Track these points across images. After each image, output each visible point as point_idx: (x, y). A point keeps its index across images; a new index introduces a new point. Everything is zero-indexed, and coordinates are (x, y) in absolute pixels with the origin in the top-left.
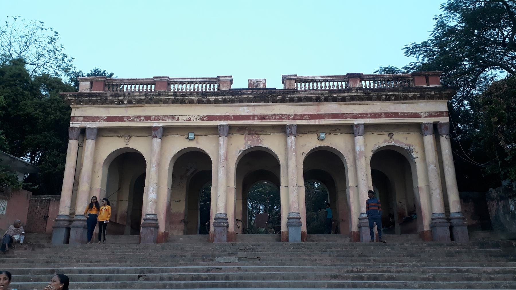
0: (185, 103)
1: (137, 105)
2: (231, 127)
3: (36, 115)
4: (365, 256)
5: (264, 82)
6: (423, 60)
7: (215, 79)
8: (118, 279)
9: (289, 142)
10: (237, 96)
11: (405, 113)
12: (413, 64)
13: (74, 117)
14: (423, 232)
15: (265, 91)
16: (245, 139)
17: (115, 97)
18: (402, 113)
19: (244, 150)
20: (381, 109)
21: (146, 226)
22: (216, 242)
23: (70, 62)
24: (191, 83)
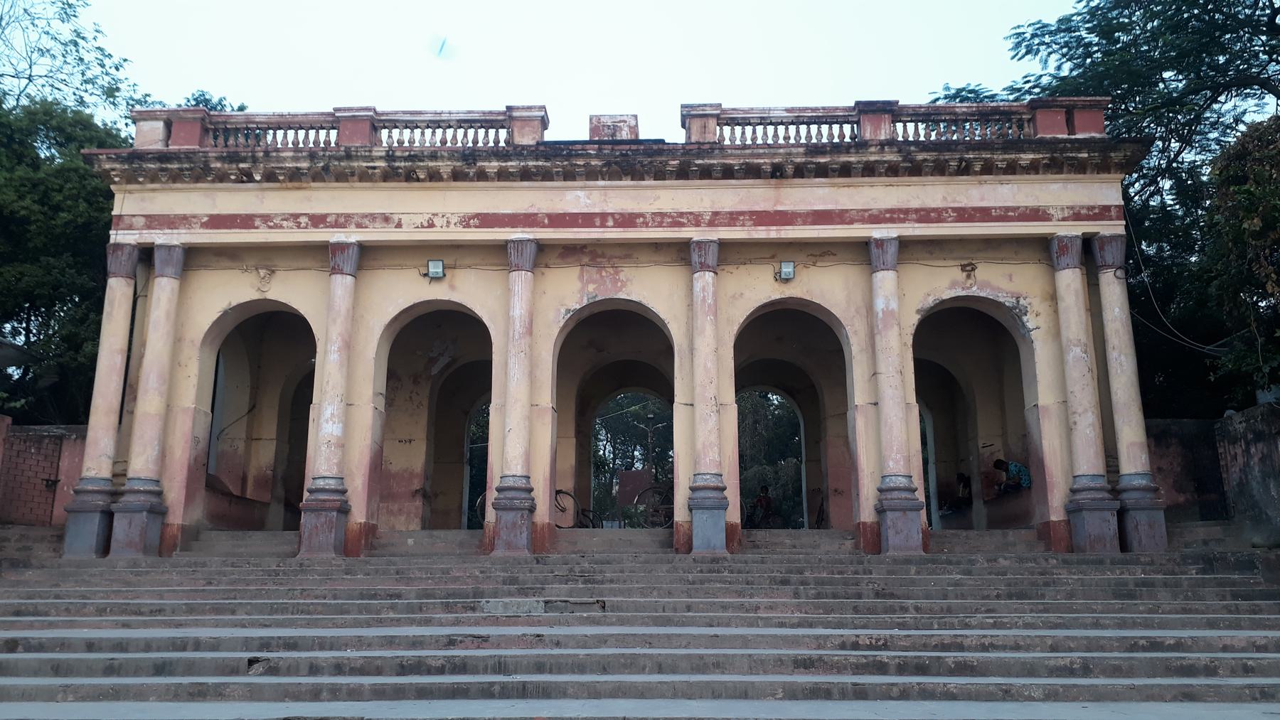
0: (418, 180)
1: (290, 185)
2: (542, 247)
3: (23, 212)
4: (892, 596)
5: (633, 123)
6: (1059, 68)
7: (499, 113)
8: (191, 668)
9: (698, 286)
10: (558, 162)
11: (1008, 209)
12: (1032, 79)
13: (120, 217)
14: (1047, 524)
15: (634, 147)
16: (581, 277)
17: (231, 162)
18: (1000, 208)
19: (578, 307)
20: (945, 198)
21: (318, 509)
22: (498, 553)
23: (117, 69)
24: (435, 124)
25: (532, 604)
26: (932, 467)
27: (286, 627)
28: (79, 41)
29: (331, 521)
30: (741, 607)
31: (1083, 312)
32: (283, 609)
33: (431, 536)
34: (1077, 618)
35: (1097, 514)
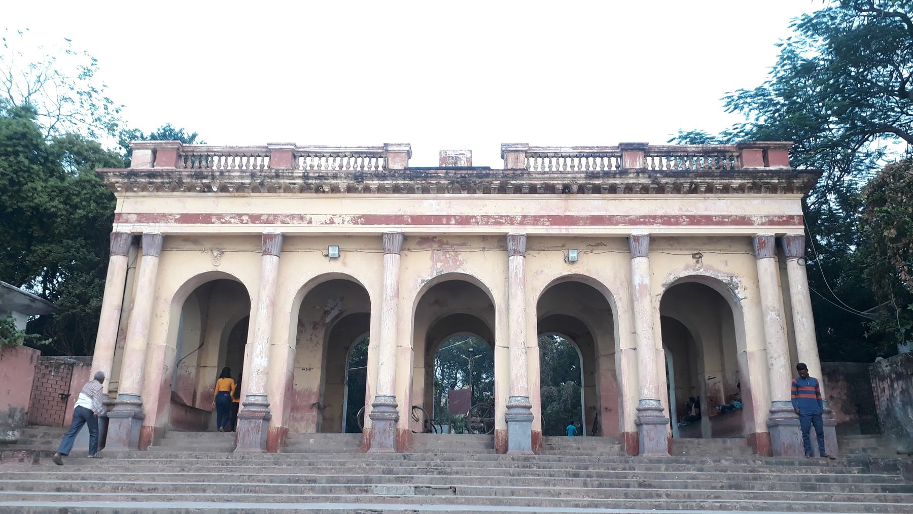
0: (324, 192)
1: (236, 194)
2: (406, 237)
3: (53, 210)
4: (650, 486)
5: (469, 156)
6: (757, 119)
7: (379, 148)
9: (512, 266)
10: (418, 180)
11: (724, 217)
12: (739, 126)
13: (120, 214)
14: (754, 435)
15: (470, 172)
16: (432, 258)
17: (197, 179)
19: (430, 278)
20: (681, 209)
21: (249, 418)
22: (373, 450)
25: (406, 488)
26: (672, 392)
27: (242, 501)
28: (93, 93)
29: (258, 426)
30: (548, 493)
31: (776, 288)
32: (238, 489)
33: (326, 438)
34: (776, 504)
35: (789, 428)
